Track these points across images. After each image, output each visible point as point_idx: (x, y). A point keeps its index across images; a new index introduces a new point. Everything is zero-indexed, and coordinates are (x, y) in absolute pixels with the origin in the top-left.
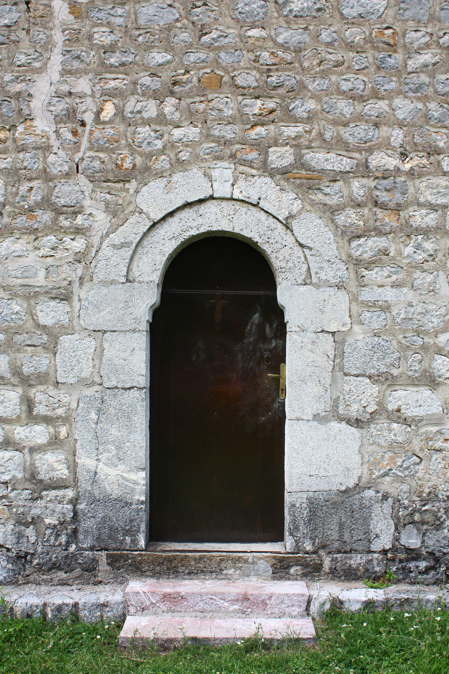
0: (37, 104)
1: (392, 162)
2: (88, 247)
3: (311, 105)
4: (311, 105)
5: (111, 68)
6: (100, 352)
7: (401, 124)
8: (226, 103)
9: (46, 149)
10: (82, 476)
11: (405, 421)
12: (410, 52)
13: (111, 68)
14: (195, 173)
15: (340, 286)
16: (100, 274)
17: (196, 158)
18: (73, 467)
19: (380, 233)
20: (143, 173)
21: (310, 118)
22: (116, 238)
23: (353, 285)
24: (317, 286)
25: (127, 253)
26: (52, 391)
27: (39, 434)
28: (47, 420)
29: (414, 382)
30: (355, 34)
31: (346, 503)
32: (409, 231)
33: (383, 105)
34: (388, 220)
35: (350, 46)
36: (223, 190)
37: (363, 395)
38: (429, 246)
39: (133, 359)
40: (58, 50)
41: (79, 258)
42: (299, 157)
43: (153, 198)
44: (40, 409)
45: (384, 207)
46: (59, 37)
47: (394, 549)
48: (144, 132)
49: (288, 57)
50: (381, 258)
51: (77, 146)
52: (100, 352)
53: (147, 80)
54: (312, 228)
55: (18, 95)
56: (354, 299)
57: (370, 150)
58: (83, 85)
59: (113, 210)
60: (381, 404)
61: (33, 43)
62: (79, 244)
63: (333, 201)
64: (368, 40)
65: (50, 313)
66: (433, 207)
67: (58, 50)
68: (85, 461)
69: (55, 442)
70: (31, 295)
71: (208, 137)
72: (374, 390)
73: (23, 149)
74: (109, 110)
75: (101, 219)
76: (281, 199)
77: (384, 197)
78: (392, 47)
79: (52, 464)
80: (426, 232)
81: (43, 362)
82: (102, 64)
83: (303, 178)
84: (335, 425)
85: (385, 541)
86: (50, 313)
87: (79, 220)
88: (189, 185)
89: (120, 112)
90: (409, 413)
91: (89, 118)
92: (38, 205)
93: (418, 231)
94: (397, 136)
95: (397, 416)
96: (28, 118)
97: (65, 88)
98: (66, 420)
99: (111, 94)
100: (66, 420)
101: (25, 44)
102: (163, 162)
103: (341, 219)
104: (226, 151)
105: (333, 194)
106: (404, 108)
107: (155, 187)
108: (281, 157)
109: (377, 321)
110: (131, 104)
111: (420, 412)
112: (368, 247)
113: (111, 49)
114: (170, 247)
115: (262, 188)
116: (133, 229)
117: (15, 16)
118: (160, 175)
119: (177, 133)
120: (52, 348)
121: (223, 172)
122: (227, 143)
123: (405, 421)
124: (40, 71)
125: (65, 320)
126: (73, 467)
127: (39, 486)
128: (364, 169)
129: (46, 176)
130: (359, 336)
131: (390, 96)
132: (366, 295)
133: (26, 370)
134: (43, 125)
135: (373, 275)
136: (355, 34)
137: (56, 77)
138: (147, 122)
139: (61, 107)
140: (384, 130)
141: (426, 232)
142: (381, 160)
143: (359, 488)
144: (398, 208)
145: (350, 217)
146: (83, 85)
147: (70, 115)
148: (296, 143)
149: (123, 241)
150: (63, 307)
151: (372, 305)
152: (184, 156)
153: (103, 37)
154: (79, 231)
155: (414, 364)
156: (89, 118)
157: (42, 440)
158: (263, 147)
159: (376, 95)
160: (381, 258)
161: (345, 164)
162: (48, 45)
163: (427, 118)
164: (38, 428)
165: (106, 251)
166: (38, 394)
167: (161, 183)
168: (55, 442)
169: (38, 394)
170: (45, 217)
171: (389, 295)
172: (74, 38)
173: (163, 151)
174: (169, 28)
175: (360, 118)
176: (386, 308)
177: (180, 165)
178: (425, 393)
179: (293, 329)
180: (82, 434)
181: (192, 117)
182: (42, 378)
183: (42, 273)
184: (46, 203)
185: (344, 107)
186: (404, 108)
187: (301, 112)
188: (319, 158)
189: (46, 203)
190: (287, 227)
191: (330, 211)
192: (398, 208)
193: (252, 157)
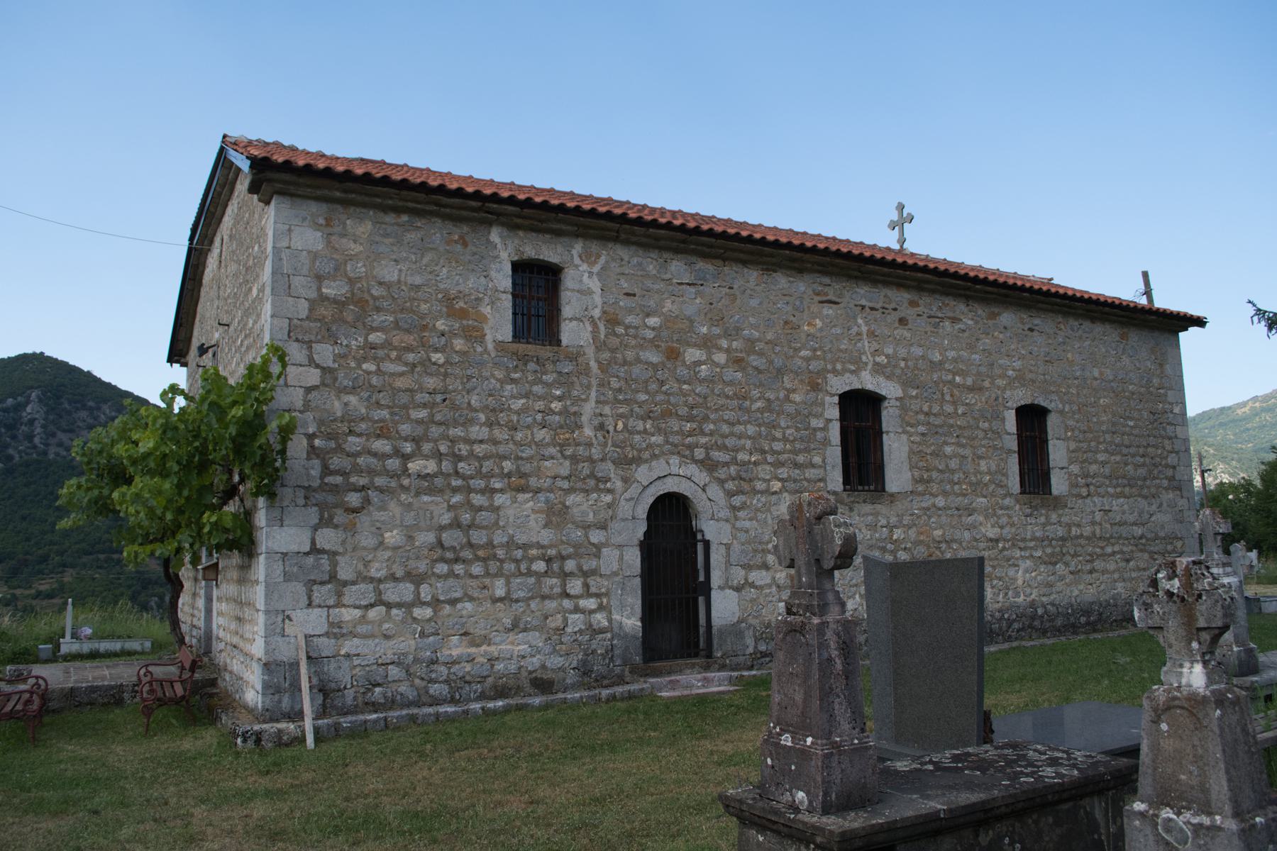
0: (584, 419)
1: (746, 458)
2: (614, 499)
3: (712, 426)
4: (712, 426)
5: (619, 402)
6: (621, 558)
7: (750, 438)
8: (674, 424)
9: (590, 445)
10: (615, 625)
11: (756, 587)
12: (753, 401)
13: (619, 402)
14: (662, 461)
15: (727, 521)
16: (620, 515)
17: (663, 453)
18: (610, 620)
19: (743, 493)
20: (638, 461)
21: (711, 434)
22: (627, 495)
23: (732, 520)
24: (717, 520)
25: (632, 503)
26: (599, 579)
27: (591, 603)
28: (597, 596)
29: (759, 568)
30: (729, 391)
31: (735, 630)
32: (755, 492)
33: (742, 427)
34: (746, 486)
35: (727, 397)
36: (675, 470)
37: (738, 575)
38: (763, 499)
39: (634, 558)
40: (594, 389)
41: (609, 506)
42: (707, 454)
43: (643, 474)
44: (593, 590)
45: (744, 480)
46: (594, 382)
47: (755, 653)
48: (637, 438)
49: (701, 401)
50: (743, 506)
51: (605, 445)
52: (621, 558)
53: (637, 409)
54: (715, 492)
55: (575, 413)
56: (734, 526)
57: (737, 451)
58: (607, 410)
59: (626, 480)
60: (746, 579)
61: (581, 385)
62: (608, 498)
63: (723, 477)
64: (735, 394)
65: (596, 537)
66: (764, 480)
67: (594, 389)
68: (616, 617)
69: (601, 608)
70: (587, 527)
71: (667, 442)
72: (743, 572)
73: (578, 445)
74: (620, 426)
75: (619, 484)
76: (701, 477)
77: (744, 475)
78: (745, 398)
79: (600, 619)
80: (762, 492)
81: (593, 563)
82: (616, 399)
83: (709, 465)
84: (728, 591)
85: (751, 650)
86: (596, 537)
87: (608, 485)
88: (659, 467)
89: (625, 426)
90: (757, 583)
91: (611, 428)
92: (588, 476)
93: (759, 492)
94: (748, 444)
95: (752, 585)
96: (580, 427)
97: (598, 411)
98: (607, 594)
99: (621, 416)
100: (607, 594)
101: (577, 387)
102: (646, 455)
103: (726, 486)
104: (676, 450)
105: (722, 473)
106: (751, 430)
107: (643, 469)
108: (699, 453)
109: (742, 537)
110: (631, 422)
111: (762, 583)
112: (737, 500)
113: (620, 390)
114: (651, 500)
115: (692, 470)
116: (634, 491)
117: (571, 367)
118: (646, 461)
119: (653, 439)
120: (598, 556)
121: (675, 460)
122: (676, 446)
123: (756, 587)
124: (586, 400)
125: (603, 540)
126: (610, 620)
127: (595, 631)
128: (734, 461)
129: (591, 460)
130: (736, 547)
131: (745, 423)
132: (738, 524)
133: (585, 568)
134: (588, 432)
135: (741, 514)
136: (729, 391)
137: (593, 404)
138: (639, 433)
139: (596, 422)
140: (743, 441)
141: (762, 492)
142: (742, 456)
143: (740, 621)
144: (751, 480)
145: (730, 485)
146: (607, 410)
147: (601, 427)
148: (707, 448)
149: (755, 777)
150: (603, 533)
151: (741, 530)
152: (657, 452)
153: (615, 383)
154: (609, 491)
155: (758, 559)
156: (611, 428)
157: (594, 607)
158: (691, 447)
159: (739, 423)
160: (743, 506)
161: (726, 458)
162: (589, 387)
163: (760, 435)
164: (592, 600)
165: (623, 503)
166: (591, 581)
167: (646, 466)
168: (601, 608)
169: (591, 581)
170: (592, 483)
171: (747, 524)
172: (601, 385)
173: (646, 449)
174: (646, 382)
175: (732, 434)
176: (747, 531)
177: (655, 457)
178: (764, 573)
179: (504, 296)
180: (614, 602)
181: (659, 430)
182: (594, 572)
183: (591, 515)
184: (592, 475)
185: (725, 429)
186: (751, 430)
187: (707, 430)
188: (716, 455)
189: (592, 475)
190: (704, 490)
191: (721, 482)
192: (751, 480)
193: (685, 452)
